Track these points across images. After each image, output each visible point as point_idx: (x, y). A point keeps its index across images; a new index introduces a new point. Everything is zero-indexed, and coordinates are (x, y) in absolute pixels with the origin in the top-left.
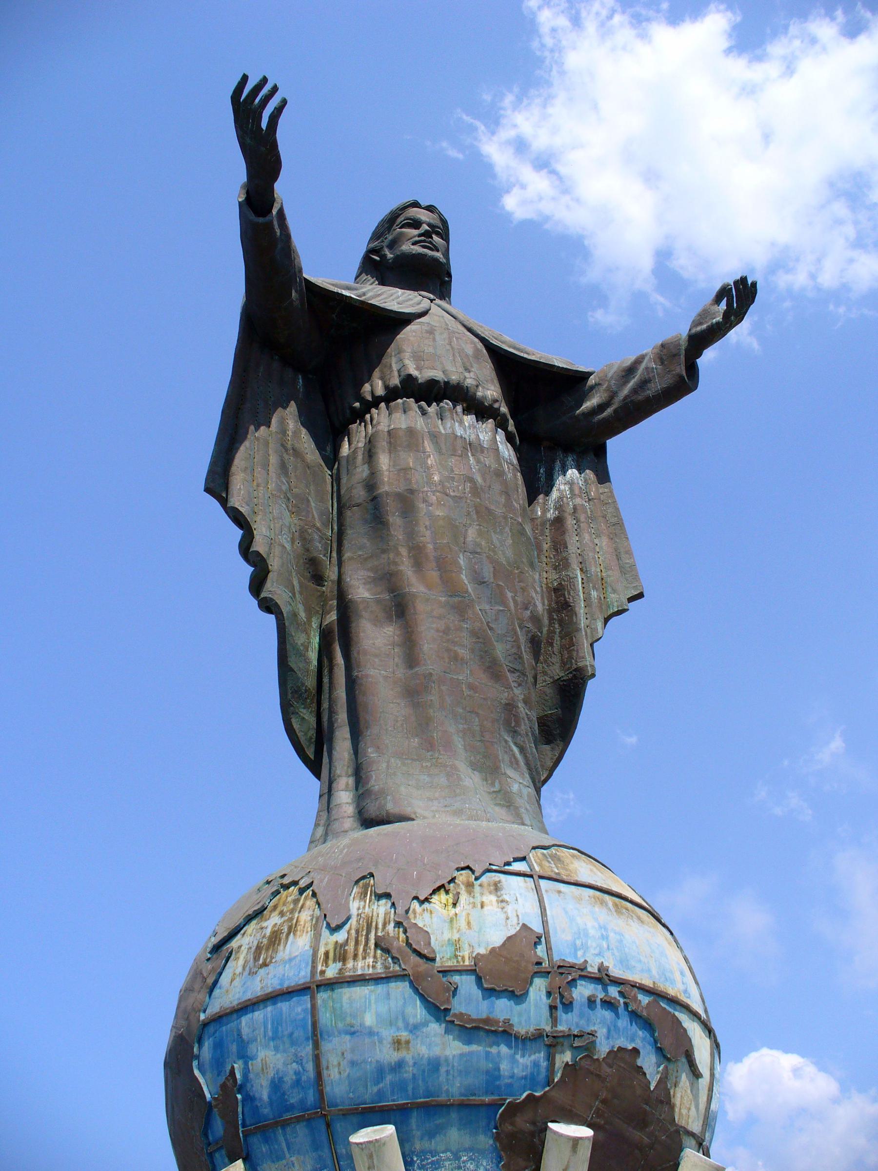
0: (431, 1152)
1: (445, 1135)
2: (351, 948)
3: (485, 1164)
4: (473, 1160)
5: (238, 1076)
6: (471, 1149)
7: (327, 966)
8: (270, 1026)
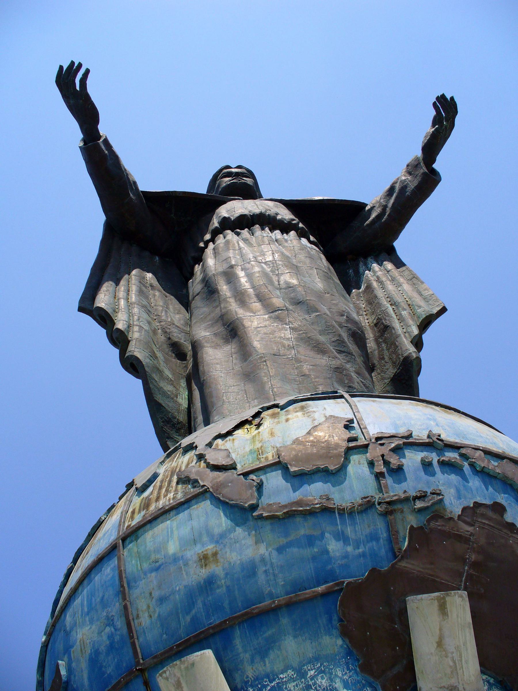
0: (268, 676)
1: (280, 649)
3: (340, 674)
4: (323, 672)
5: (63, 672)
6: (317, 659)
8: (85, 602)
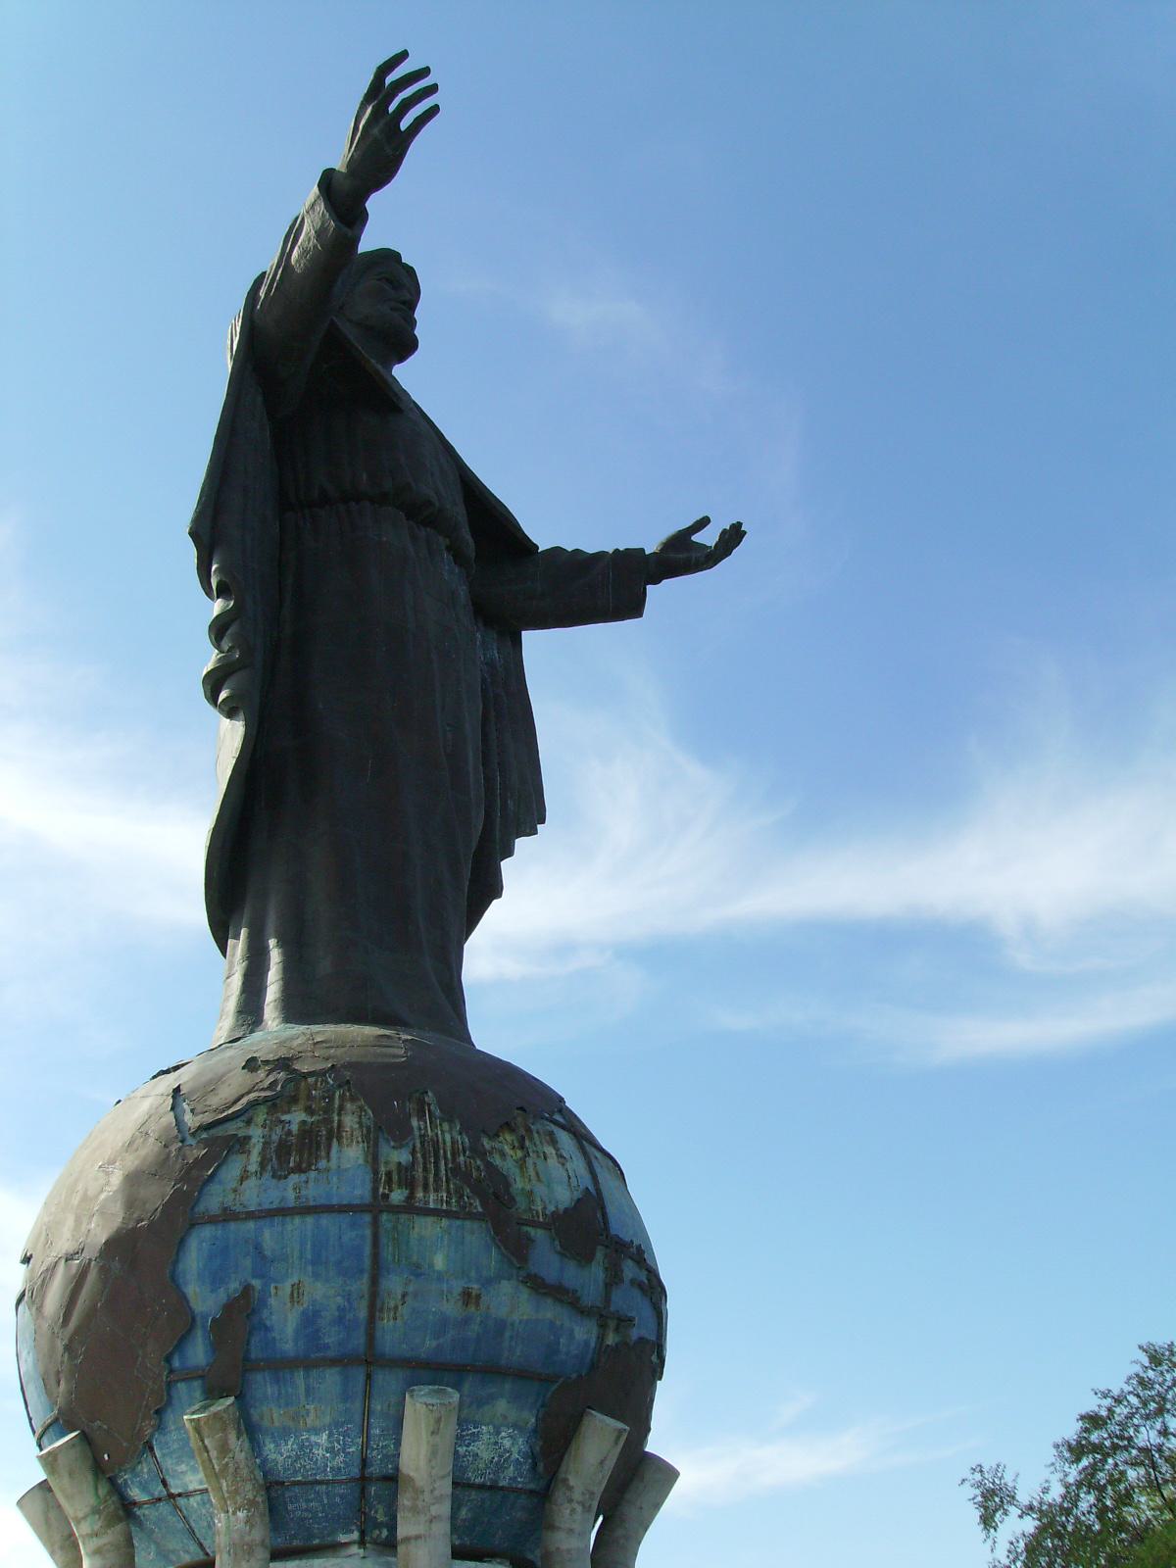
2: (419, 1173)
7: (391, 1191)
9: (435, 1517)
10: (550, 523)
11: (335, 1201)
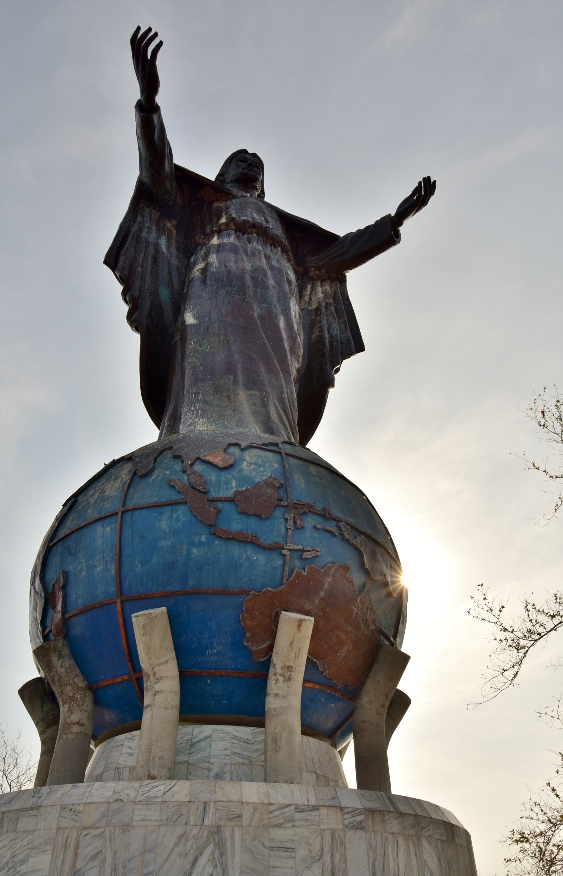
9: (157, 692)
10: (342, 221)
11: (103, 514)
